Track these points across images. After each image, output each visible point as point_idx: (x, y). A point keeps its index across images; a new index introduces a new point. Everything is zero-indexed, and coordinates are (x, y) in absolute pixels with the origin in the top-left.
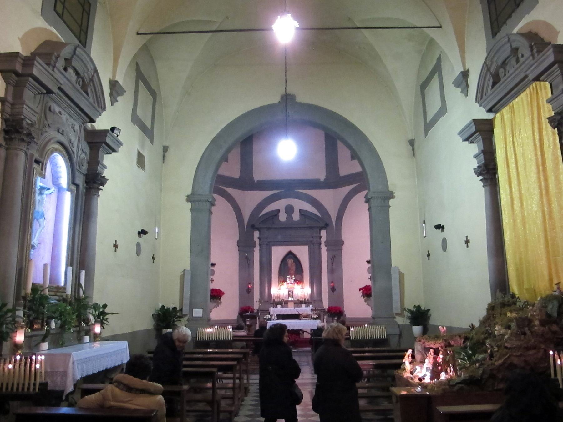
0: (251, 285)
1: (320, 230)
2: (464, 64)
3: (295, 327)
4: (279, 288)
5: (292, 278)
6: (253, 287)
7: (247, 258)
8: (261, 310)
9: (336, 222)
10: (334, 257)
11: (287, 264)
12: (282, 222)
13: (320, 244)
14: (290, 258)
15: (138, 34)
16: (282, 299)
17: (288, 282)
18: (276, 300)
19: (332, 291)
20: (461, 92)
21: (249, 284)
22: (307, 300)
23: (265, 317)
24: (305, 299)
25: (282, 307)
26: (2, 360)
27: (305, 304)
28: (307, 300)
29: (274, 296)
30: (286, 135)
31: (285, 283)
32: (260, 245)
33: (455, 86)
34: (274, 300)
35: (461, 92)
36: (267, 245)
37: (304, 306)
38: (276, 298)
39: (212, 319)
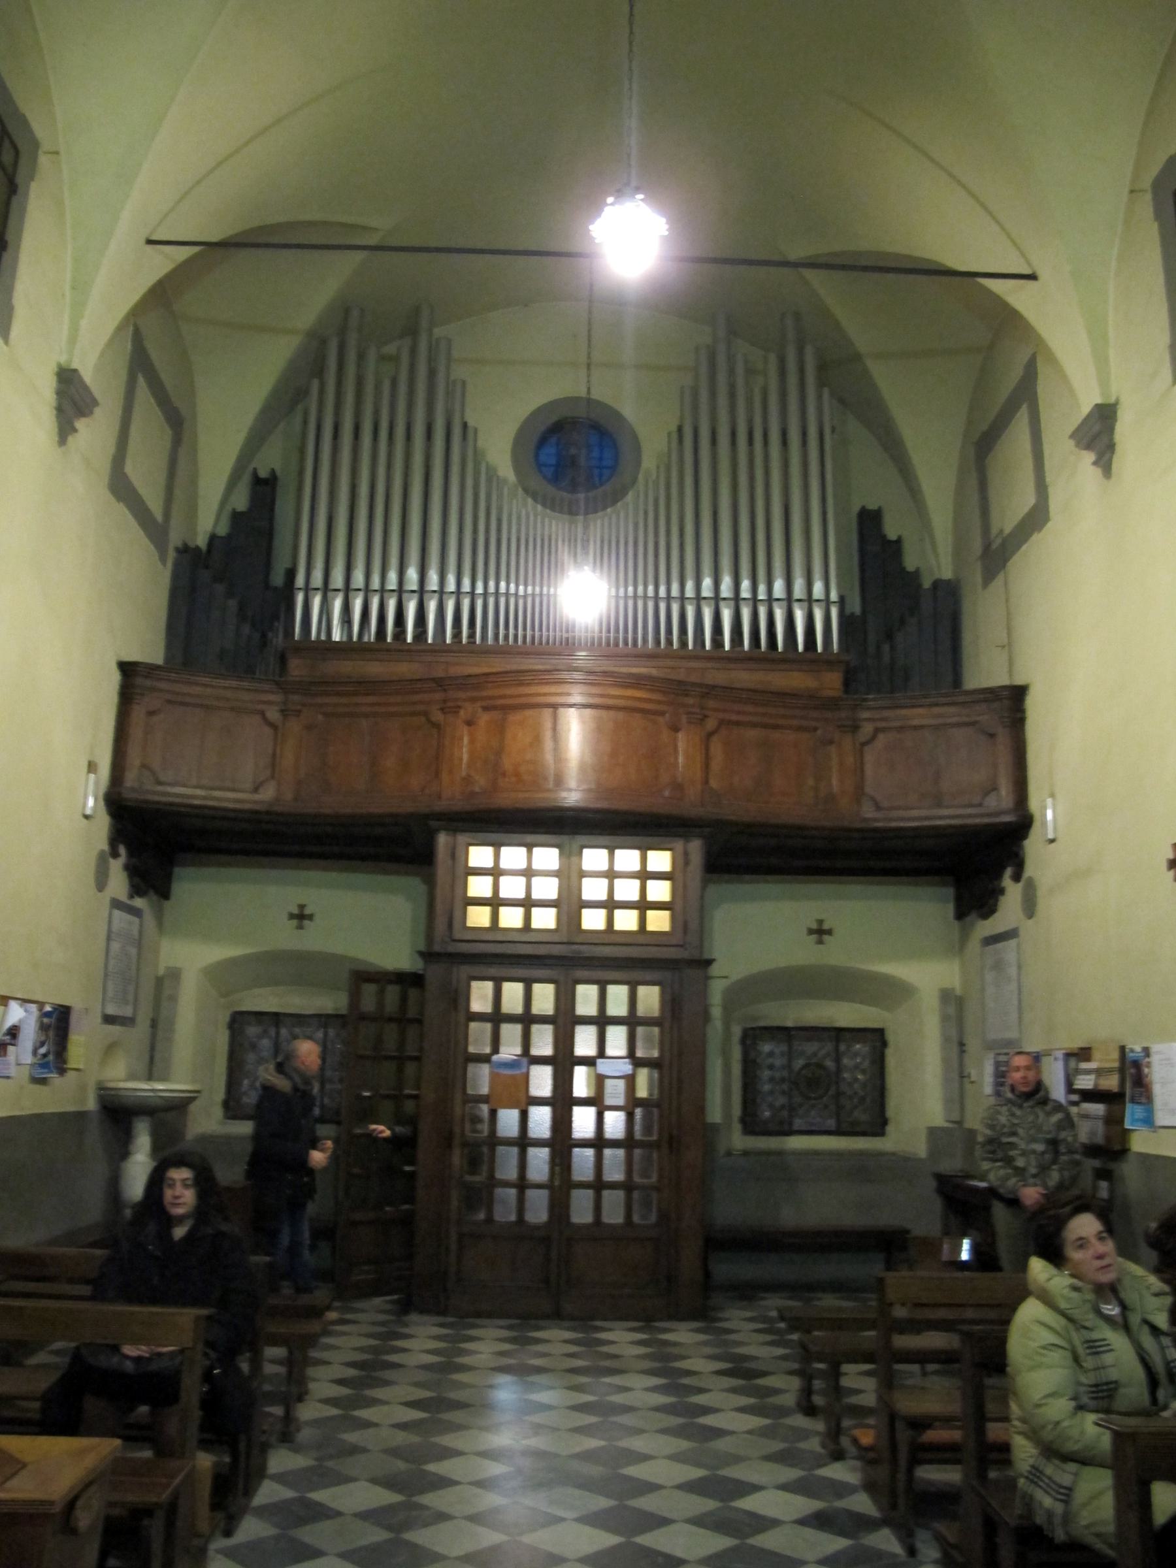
2: (1104, 381)
12: (604, 207)
15: (150, 242)
20: (1095, 463)
26: (467, 641)
30: (566, 759)
33: (1078, 445)
35: (1095, 463)
39: (572, 566)
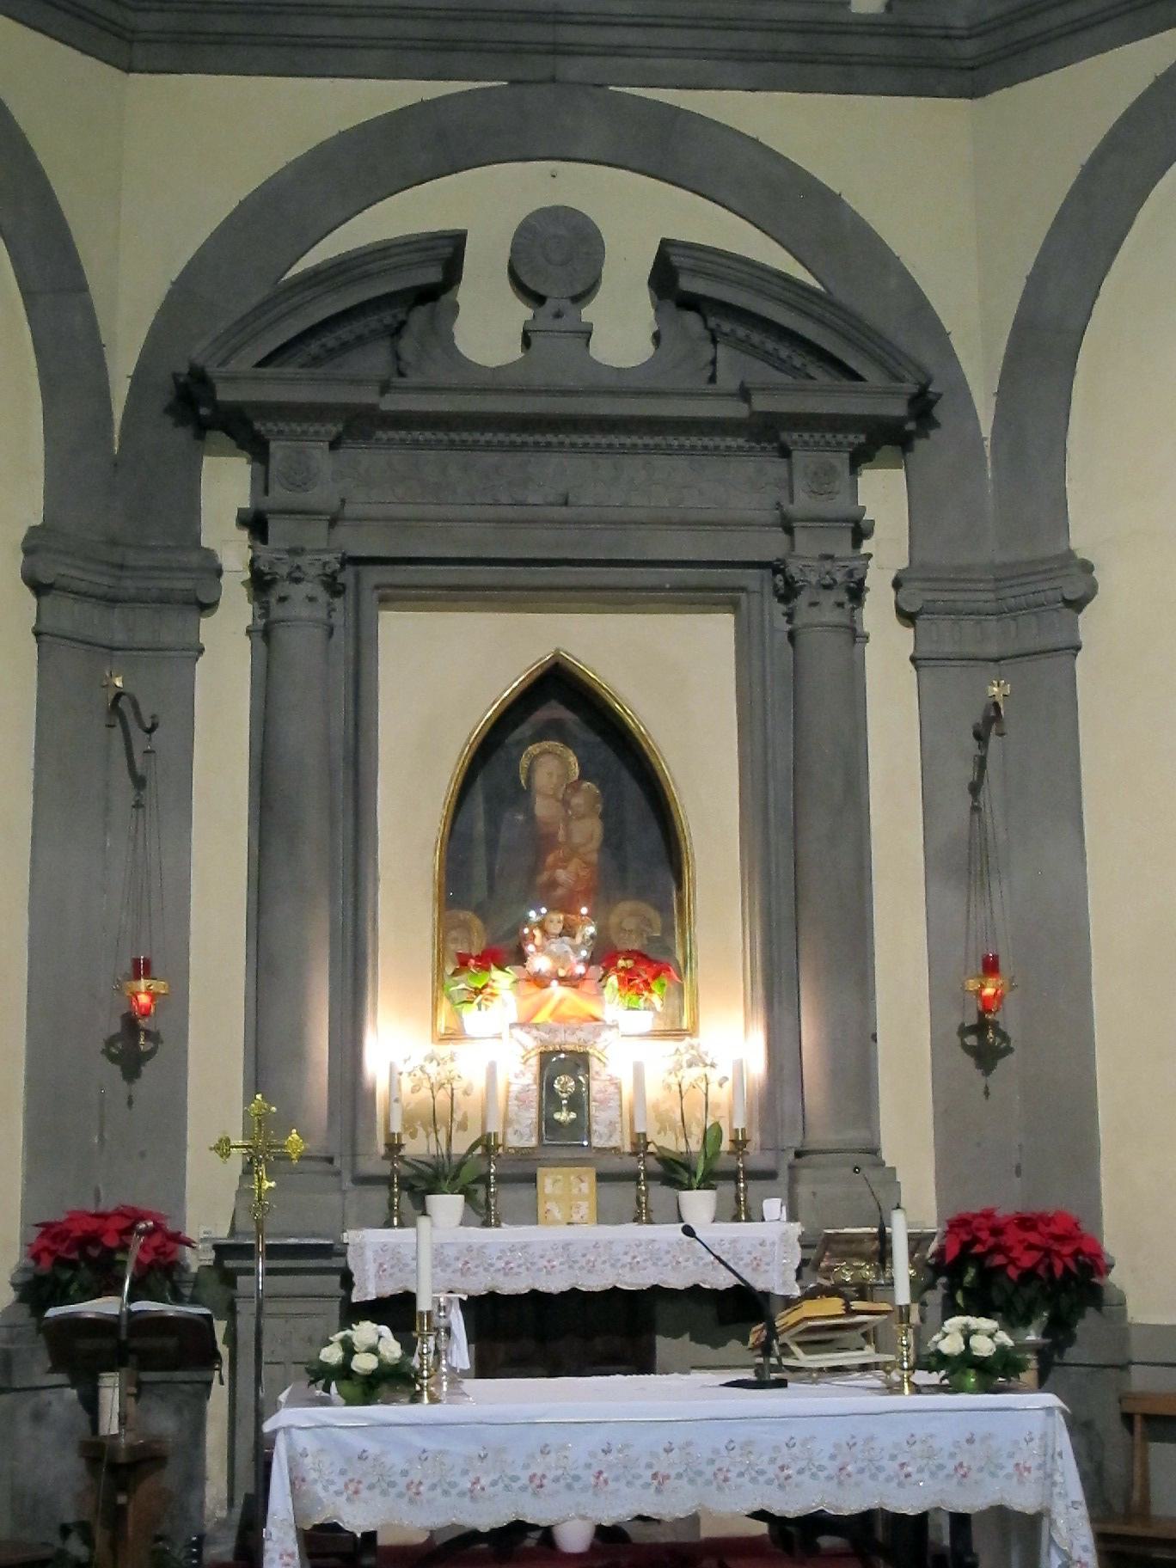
0: (159, 986)
1: (860, 458)
3: (722, 1480)
4: (441, 1027)
5: (568, 931)
6: (176, 1001)
7: (118, 708)
8: (273, 1251)
9: (1000, 406)
10: (989, 723)
11: (521, 795)
13: (857, 593)
14: (554, 730)
16: (474, 1134)
17: (539, 963)
18: (418, 1147)
19: (970, 1062)
21: (142, 969)
22: (726, 1145)
23: (332, 1355)
24: (712, 1135)
25: (482, 1213)
27: (708, 1182)
28: (726, 1145)
29: (393, 1098)
31: (502, 979)
32: (260, 583)
34: (393, 1147)
36: (334, 587)
37: (699, 1204)
38: (409, 1120)
